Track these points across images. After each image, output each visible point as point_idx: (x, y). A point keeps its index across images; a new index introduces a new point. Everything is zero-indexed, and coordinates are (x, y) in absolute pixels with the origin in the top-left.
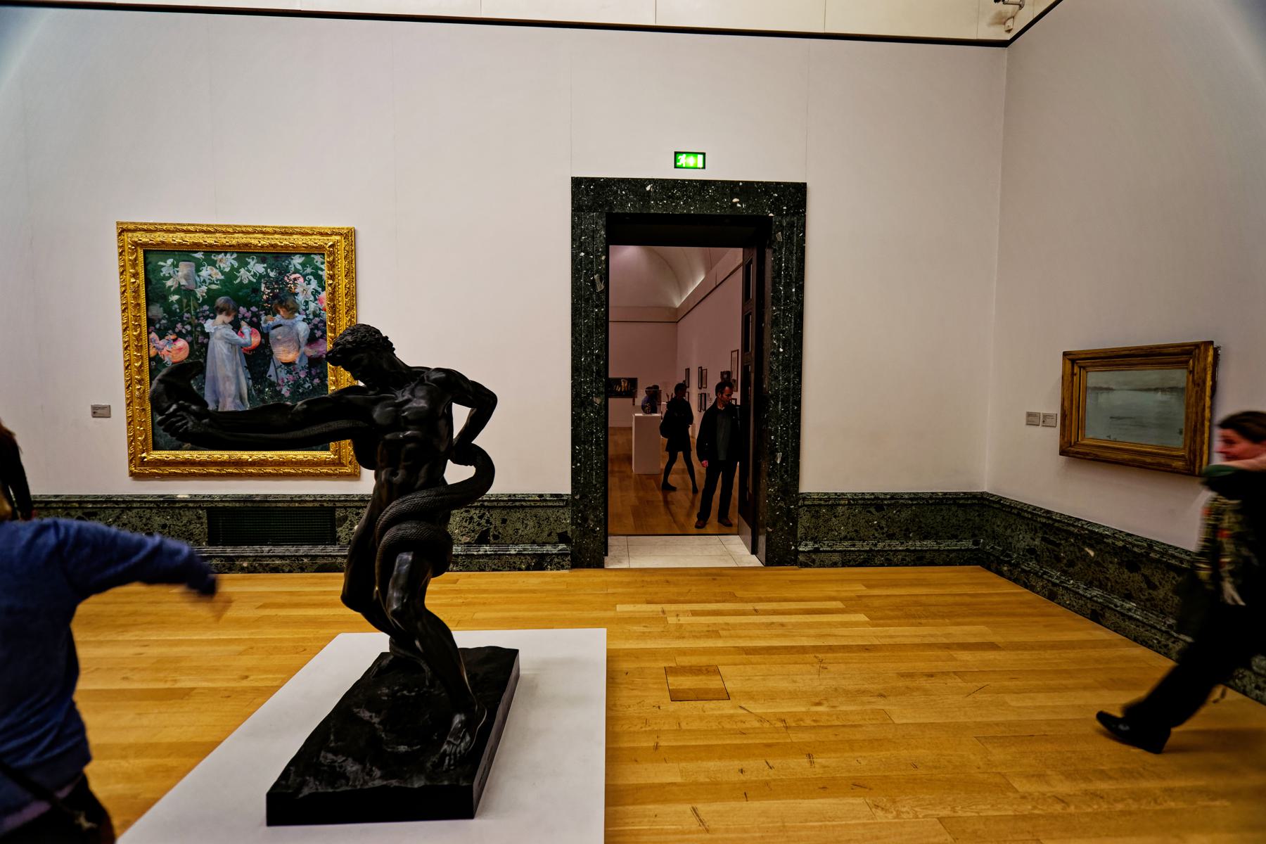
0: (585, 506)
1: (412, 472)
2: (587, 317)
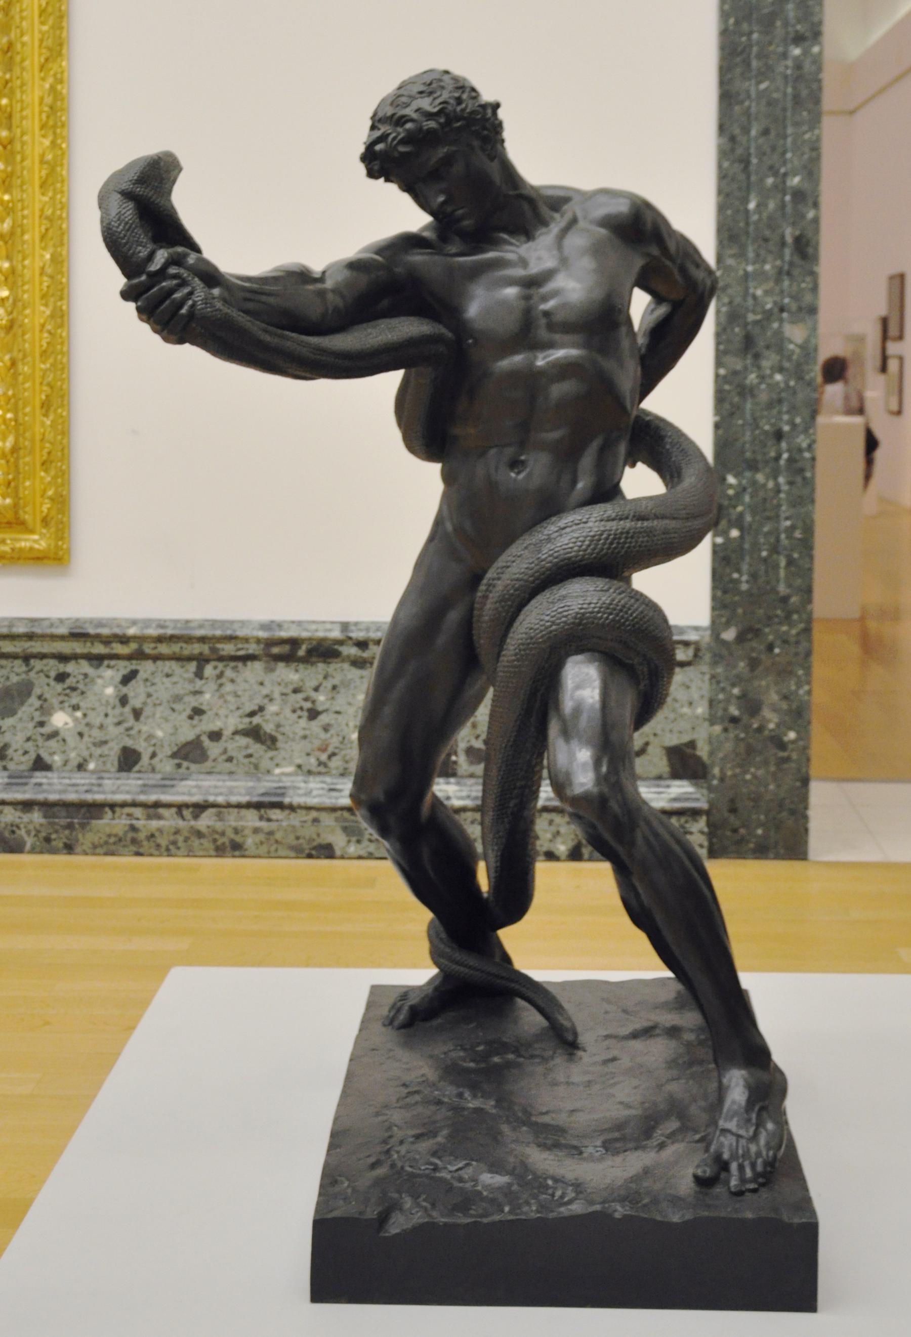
0: (754, 664)
1: (567, 456)
2: (765, 73)
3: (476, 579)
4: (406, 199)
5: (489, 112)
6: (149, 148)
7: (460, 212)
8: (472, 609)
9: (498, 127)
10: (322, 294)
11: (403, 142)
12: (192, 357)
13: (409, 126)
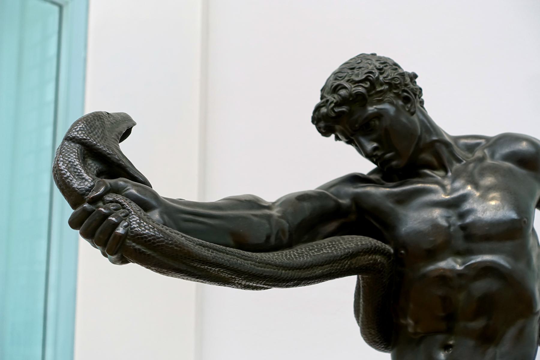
4: (351, 149)
5: (408, 80)
6: (111, 106)
7: (388, 155)
9: (418, 92)
10: (269, 217)
11: (337, 105)
13: (343, 92)
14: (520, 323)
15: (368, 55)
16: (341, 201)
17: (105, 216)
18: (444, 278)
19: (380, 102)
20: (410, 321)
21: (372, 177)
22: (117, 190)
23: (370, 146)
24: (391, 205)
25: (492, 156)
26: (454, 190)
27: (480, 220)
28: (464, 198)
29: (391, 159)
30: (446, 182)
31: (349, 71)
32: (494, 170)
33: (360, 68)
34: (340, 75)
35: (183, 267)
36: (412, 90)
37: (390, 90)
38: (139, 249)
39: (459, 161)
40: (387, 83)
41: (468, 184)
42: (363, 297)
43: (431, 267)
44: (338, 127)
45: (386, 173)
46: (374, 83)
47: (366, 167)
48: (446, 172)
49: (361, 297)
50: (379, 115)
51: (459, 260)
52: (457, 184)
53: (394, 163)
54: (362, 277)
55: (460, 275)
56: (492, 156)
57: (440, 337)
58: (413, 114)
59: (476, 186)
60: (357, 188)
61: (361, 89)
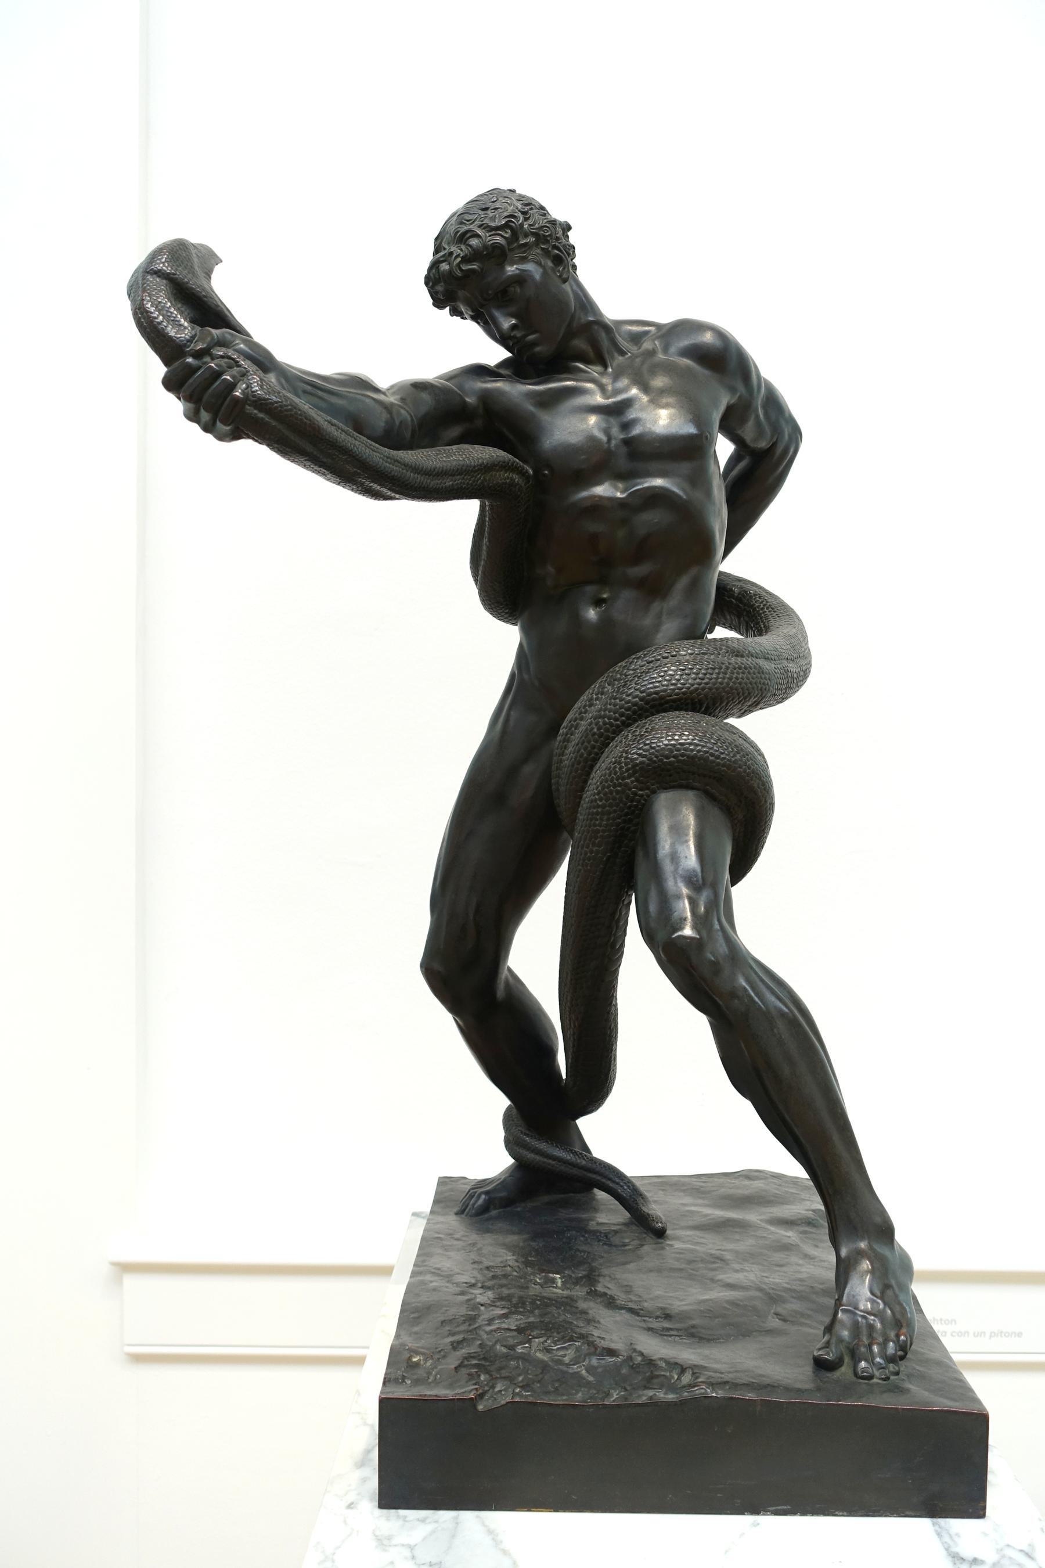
3: (553, 730)
8: (549, 765)
11: (466, 260)
12: (441, 1025)
13: (474, 242)
14: (694, 571)
15: (505, 191)
16: (467, 399)
17: (218, 374)
18: (598, 508)
19: (523, 260)
20: (551, 569)
21: (502, 371)
22: (222, 343)
23: (507, 323)
24: (532, 408)
25: (666, 349)
26: (617, 392)
27: (651, 433)
28: (628, 403)
29: (534, 344)
30: (605, 380)
31: (481, 212)
32: (669, 368)
33: (496, 209)
34: (467, 217)
35: (309, 448)
36: (564, 246)
37: (536, 244)
38: (262, 419)
39: (622, 353)
40: (533, 234)
41: (635, 384)
42: (489, 534)
43: (584, 494)
44: (461, 293)
45: (519, 367)
46: (516, 233)
47: (495, 354)
48: (606, 367)
49: (486, 534)
50: (521, 279)
51: (620, 485)
52: (623, 382)
53: (538, 349)
54: (491, 506)
55: (621, 504)
56: (666, 349)
57: (590, 589)
58: (565, 281)
59: (645, 388)
60: (485, 382)
61: (498, 239)
